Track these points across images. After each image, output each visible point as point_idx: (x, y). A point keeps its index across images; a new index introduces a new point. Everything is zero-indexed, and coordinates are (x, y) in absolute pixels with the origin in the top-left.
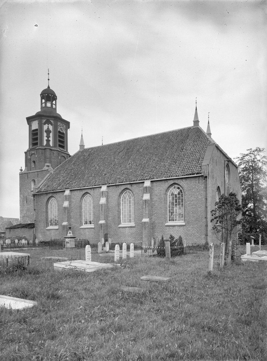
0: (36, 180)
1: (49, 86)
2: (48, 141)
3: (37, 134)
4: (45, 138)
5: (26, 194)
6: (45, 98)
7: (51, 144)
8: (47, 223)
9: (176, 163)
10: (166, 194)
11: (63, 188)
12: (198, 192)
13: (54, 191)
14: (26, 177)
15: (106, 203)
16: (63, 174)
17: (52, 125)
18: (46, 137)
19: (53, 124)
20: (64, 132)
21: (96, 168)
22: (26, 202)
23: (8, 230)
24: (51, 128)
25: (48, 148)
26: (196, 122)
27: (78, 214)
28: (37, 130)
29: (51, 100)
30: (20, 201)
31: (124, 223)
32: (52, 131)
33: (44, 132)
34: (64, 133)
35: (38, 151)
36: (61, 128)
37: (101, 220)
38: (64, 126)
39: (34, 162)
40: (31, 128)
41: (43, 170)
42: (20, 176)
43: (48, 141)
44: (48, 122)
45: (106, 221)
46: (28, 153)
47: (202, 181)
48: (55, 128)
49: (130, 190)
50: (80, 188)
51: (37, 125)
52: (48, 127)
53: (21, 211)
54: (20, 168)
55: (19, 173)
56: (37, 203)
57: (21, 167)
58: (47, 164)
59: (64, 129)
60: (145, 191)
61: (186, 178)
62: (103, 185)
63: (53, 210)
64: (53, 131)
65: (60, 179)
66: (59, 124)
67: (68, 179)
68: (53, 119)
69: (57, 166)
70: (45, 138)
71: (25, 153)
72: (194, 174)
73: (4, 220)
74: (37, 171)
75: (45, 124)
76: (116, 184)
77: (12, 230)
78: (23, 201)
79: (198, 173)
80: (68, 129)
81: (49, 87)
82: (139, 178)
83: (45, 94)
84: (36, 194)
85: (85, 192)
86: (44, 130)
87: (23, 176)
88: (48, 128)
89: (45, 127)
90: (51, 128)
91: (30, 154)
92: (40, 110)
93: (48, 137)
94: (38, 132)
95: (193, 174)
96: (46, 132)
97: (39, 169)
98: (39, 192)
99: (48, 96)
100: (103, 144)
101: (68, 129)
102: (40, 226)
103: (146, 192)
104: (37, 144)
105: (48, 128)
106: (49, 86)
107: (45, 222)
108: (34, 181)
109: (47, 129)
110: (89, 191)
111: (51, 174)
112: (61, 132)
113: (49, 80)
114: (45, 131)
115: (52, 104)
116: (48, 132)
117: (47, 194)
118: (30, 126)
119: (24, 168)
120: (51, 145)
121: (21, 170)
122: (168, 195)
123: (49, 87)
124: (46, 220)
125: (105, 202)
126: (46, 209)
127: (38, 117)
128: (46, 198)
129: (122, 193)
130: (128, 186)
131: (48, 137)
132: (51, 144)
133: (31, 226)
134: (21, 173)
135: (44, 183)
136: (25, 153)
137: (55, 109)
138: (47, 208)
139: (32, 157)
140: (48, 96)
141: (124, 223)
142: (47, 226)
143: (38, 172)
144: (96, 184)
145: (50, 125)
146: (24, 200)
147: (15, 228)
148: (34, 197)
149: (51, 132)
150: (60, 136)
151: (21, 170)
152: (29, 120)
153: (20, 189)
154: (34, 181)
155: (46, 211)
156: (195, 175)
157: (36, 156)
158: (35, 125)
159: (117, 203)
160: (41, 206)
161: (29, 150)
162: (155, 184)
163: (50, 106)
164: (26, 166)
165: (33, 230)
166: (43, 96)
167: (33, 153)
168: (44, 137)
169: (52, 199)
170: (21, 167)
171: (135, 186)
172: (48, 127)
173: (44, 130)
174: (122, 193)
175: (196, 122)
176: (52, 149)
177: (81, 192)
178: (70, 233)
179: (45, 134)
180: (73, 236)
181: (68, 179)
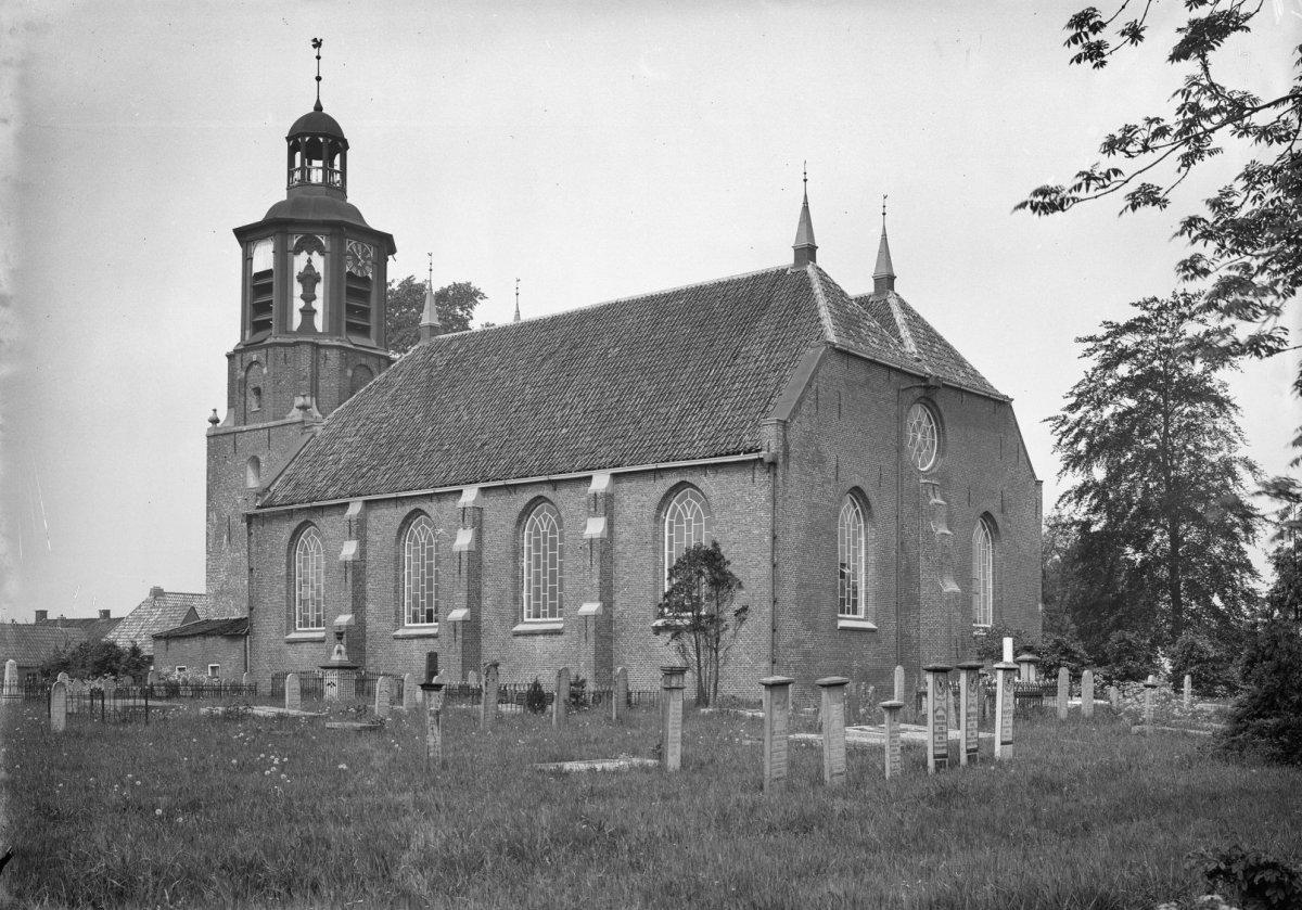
0: (262, 458)
1: (318, 101)
2: (308, 313)
3: (268, 289)
4: (298, 303)
5: (228, 510)
6: (303, 148)
7: (319, 323)
8: (288, 617)
9: (701, 408)
10: (657, 518)
11: (343, 493)
12: (749, 514)
13: (315, 504)
14: (230, 449)
15: (474, 549)
16: (350, 440)
17: (322, 253)
18: (302, 297)
19: (328, 249)
20: (370, 276)
21: (458, 420)
22: (229, 539)
23: (163, 642)
24: (319, 263)
25: (307, 343)
26: (806, 252)
27: (391, 585)
28: (268, 273)
29: (325, 152)
30: (208, 534)
31: (532, 620)
32: (322, 275)
33: (295, 281)
34: (367, 277)
35: (270, 351)
36: (358, 259)
37: (454, 608)
38: (367, 252)
39: (258, 391)
40: (249, 267)
41: (287, 421)
42: (208, 443)
43: (308, 313)
44: (309, 244)
45: (604, 606)
46: (238, 358)
47: (761, 477)
48: (335, 265)
49: (552, 504)
50: (394, 495)
51: (271, 256)
52: (309, 261)
53: (211, 573)
54: (211, 414)
55: (204, 432)
56: (258, 544)
57: (215, 410)
58: (299, 401)
59: (369, 262)
60: (593, 509)
61: (716, 464)
62: (467, 483)
63: (689, 525)
64: (325, 274)
65: (340, 459)
66: (350, 245)
67: (364, 459)
68: (328, 231)
69: (340, 404)
70: (298, 303)
71: (230, 356)
72: (739, 453)
73: (170, 603)
74: (265, 425)
75: (297, 251)
76: (509, 482)
77: (174, 644)
78: (218, 537)
79: (750, 451)
80: (390, 257)
81: (318, 107)
82: (580, 461)
83: (303, 135)
84: (256, 515)
85: (413, 507)
86: (296, 274)
87: (218, 441)
88: (309, 266)
89: (299, 263)
90: (319, 263)
91: (246, 364)
92: (282, 196)
93: (309, 297)
94: (274, 280)
95: (734, 454)
96: (300, 279)
97: (275, 419)
98: (266, 507)
99: (317, 139)
100: (526, 317)
101: (390, 257)
102: (268, 631)
103: (595, 515)
104: (266, 325)
105: (309, 266)
106: (318, 101)
107: (284, 615)
108: (255, 462)
109: (306, 268)
110: (424, 506)
111: (313, 436)
112: (359, 274)
113: (319, 79)
114: (298, 277)
115: (328, 170)
116: (309, 278)
117: (290, 513)
118: (247, 259)
119: (222, 415)
120: (320, 329)
121: (215, 421)
122: (666, 524)
123: (318, 107)
124: (288, 607)
125: (469, 545)
126: (288, 567)
127: (274, 226)
128: (285, 530)
129: (526, 512)
130: (546, 492)
131: (309, 297)
132: (319, 323)
133: (235, 630)
134: (212, 433)
135: (287, 472)
136: (230, 356)
137: (343, 190)
138: (290, 564)
139: (251, 373)
140: (317, 139)
141: (532, 620)
142: (291, 627)
143: (269, 428)
144: (448, 480)
145: (315, 254)
146: (219, 531)
147: (186, 636)
148: (249, 524)
149: (317, 279)
150: (351, 292)
151: (215, 421)
152: (247, 236)
153: (208, 492)
154: (255, 462)
155: (288, 574)
156: (742, 457)
157: (265, 371)
158: (264, 257)
159: (510, 549)
160: (271, 556)
161: (242, 347)
162: (625, 485)
163: (320, 180)
164: (231, 405)
165: (243, 643)
166: (296, 142)
167: (254, 358)
168: (295, 299)
169: (309, 533)
170: (215, 410)
171: (564, 492)
172: (309, 261)
173: (296, 274)
174: (526, 512)
175: (806, 252)
176: (322, 342)
177: (399, 510)
178: (339, 652)
179: (298, 289)
180: (349, 664)
181: (364, 459)
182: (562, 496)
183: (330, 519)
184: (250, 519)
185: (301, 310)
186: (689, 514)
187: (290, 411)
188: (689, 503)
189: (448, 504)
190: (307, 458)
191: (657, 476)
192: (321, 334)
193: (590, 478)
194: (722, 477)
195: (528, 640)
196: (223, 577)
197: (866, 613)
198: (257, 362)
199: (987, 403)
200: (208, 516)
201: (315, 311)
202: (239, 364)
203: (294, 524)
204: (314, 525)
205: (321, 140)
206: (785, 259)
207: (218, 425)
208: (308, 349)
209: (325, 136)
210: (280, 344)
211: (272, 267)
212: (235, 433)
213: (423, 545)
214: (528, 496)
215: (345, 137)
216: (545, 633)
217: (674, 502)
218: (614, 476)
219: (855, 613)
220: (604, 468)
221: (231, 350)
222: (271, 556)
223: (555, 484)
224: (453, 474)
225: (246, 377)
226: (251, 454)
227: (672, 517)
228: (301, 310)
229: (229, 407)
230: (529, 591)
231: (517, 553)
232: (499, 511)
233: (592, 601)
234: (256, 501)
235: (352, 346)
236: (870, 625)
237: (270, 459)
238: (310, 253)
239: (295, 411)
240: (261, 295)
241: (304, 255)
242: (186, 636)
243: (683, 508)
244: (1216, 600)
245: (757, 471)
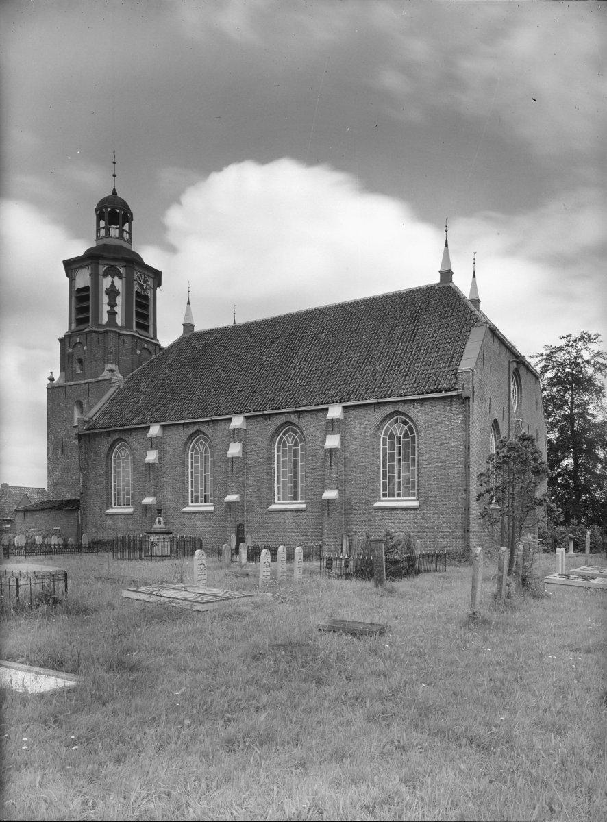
0: (84, 402)
1: (114, 189)
2: (112, 314)
3: (86, 298)
6: (106, 217)
7: (119, 320)
8: (107, 498)
13: (125, 427)
14: (63, 396)
17: (120, 278)
18: (109, 304)
19: (124, 275)
22: (62, 451)
24: (119, 284)
31: (281, 502)
32: (120, 291)
39: (80, 361)
40: (73, 285)
43: (112, 314)
46: (67, 340)
49: (205, 435)
52: (113, 282)
53: (51, 471)
54: (50, 375)
57: (52, 373)
58: (110, 366)
62: (235, 413)
68: (124, 264)
72: (441, 391)
74: (86, 381)
75: (105, 276)
76: (266, 412)
78: (56, 449)
79: (449, 390)
81: (114, 193)
84: (84, 435)
88: (113, 285)
89: (106, 283)
90: (119, 284)
92: (93, 244)
93: (112, 304)
96: (107, 293)
101: (158, 288)
105: (113, 285)
106: (114, 189)
115: (122, 231)
116: (112, 293)
117: (109, 433)
119: (57, 376)
121: (52, 379)
122: (381, 439)
123: (114, 193)
127: (91, 258)
129: (190, 438)
130: (293, 418)
131: (112, 304)
132: (119, 320)
134: (50, 386)
136: (61, 340)
143: (88, 383)
147: (37, 510)
149: (118, 294)
151: (52, 379)
152: (71, 266)
156: (443, 394)
161: (69, 333)
162: (352, 413)
163: (117, 236)
164: (63, 369)
165: (76, 514)
167: (78, 340)
168: (104, 305)
171: (307, 418)
172: (113, 282)
173: (104, 289)
176: (121, 332)
178: (159, 522)
182: (306, 423)
183: (171, 433)
184: (80, 437)
185: (108, 312)
186: (290, 442)
187: (102, 373)
188: (123, 449)
189: (221, 427)
190: (115, 401)
191: (377, 407)
192: (121, 327)
193: (327, 409)
194: (427, 408)
195: (279, 515)
196: (59, 474)
198: (80, 343)
199: (258, 419)
200: (48, 437)
201: (116, 313)
202: (68, 344)
203: (111, 440)
204: (124, 440)
205: (118, 211)
206: (435, 279)
207: (54, 382)
208: (113, 335)
209: (121, 209)
210: (94, 332)
211: (89, 285)
212: (66, 386)
213: (202, 453)
214: (279, 421)
215: (132, 211)
216: (292, 511)
217: (116, 449)
218: (344, 407)
220: (337, 402)
221: (62, 336)
222: (95, 460)
224: (222, 408)
226: (76, 399)
227: (192, 451)
228: (108, 312)
229: (61, 371)
230: (278, 483)
231: (270, 460)
232: (257, 432)
233: (331, 489)
234: (84, 426)
235: (139, 336)
237: (89, 402)
239: (105, 373)
240: (82, 302)
241: (109, 279)
242: (37, 510)
243: (120, 452)
245: (454, 406)
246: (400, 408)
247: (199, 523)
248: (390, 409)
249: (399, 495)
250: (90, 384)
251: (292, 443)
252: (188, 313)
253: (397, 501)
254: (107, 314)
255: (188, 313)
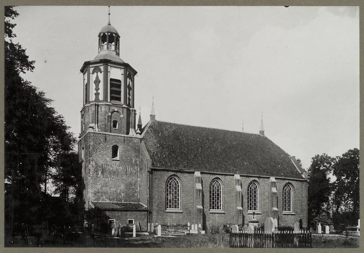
1: (109, 22)
2: (97, 94)
43: (97, 94)
52: (97, 75)
99: (15, 25)
106: (109, 22)
130: (256, 179)
139: (113, 115)
140: (15, 25)
145: (99, 73)
167: (116, 110)
171: (262, 179)
172: (97, 75)
185: (95, 94)
186: (173, 183)
193: (234, 175)
197: (293, 211)
219: (289, 210)
223: (259, 177)
225: (111, 116)
228: (95, 94)
236: (181, 211)
238: (97, 73)
244: (71, 196)
246: (290, 181)
247: (217, 218)
248: (287, 181)
249: (173, 208)
250: (107, 135)
251: (174, 183)
252: (153, 110)
253: (169, 210)
254: (94, 95)
255: (153, 110)
